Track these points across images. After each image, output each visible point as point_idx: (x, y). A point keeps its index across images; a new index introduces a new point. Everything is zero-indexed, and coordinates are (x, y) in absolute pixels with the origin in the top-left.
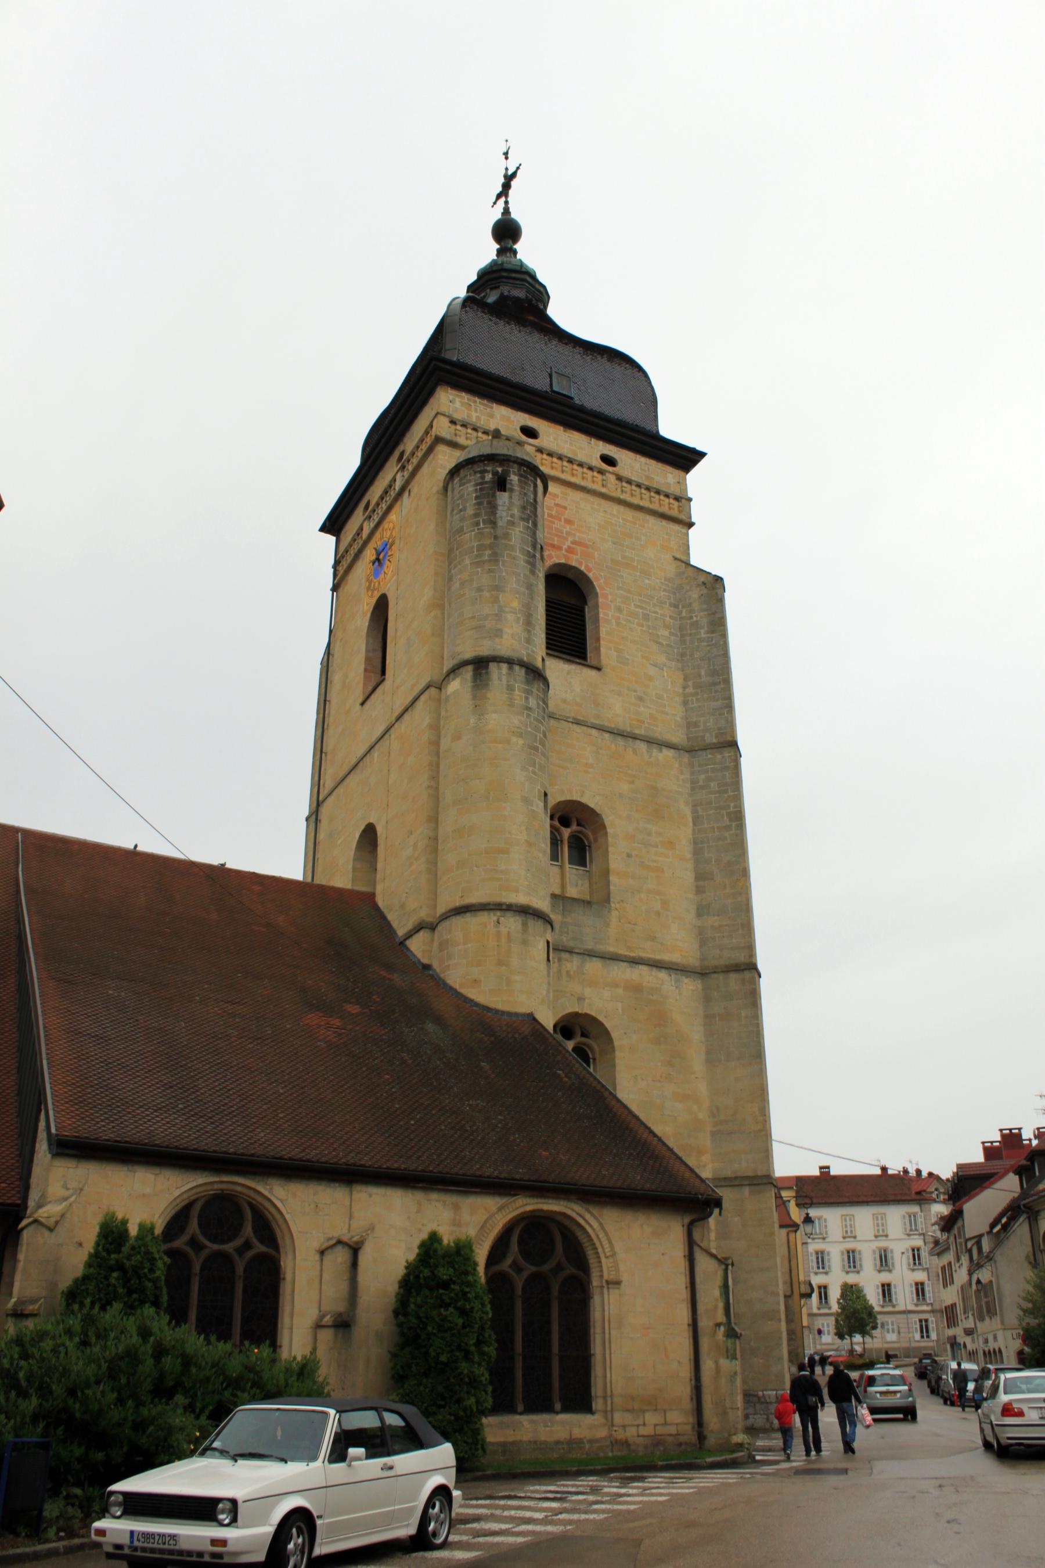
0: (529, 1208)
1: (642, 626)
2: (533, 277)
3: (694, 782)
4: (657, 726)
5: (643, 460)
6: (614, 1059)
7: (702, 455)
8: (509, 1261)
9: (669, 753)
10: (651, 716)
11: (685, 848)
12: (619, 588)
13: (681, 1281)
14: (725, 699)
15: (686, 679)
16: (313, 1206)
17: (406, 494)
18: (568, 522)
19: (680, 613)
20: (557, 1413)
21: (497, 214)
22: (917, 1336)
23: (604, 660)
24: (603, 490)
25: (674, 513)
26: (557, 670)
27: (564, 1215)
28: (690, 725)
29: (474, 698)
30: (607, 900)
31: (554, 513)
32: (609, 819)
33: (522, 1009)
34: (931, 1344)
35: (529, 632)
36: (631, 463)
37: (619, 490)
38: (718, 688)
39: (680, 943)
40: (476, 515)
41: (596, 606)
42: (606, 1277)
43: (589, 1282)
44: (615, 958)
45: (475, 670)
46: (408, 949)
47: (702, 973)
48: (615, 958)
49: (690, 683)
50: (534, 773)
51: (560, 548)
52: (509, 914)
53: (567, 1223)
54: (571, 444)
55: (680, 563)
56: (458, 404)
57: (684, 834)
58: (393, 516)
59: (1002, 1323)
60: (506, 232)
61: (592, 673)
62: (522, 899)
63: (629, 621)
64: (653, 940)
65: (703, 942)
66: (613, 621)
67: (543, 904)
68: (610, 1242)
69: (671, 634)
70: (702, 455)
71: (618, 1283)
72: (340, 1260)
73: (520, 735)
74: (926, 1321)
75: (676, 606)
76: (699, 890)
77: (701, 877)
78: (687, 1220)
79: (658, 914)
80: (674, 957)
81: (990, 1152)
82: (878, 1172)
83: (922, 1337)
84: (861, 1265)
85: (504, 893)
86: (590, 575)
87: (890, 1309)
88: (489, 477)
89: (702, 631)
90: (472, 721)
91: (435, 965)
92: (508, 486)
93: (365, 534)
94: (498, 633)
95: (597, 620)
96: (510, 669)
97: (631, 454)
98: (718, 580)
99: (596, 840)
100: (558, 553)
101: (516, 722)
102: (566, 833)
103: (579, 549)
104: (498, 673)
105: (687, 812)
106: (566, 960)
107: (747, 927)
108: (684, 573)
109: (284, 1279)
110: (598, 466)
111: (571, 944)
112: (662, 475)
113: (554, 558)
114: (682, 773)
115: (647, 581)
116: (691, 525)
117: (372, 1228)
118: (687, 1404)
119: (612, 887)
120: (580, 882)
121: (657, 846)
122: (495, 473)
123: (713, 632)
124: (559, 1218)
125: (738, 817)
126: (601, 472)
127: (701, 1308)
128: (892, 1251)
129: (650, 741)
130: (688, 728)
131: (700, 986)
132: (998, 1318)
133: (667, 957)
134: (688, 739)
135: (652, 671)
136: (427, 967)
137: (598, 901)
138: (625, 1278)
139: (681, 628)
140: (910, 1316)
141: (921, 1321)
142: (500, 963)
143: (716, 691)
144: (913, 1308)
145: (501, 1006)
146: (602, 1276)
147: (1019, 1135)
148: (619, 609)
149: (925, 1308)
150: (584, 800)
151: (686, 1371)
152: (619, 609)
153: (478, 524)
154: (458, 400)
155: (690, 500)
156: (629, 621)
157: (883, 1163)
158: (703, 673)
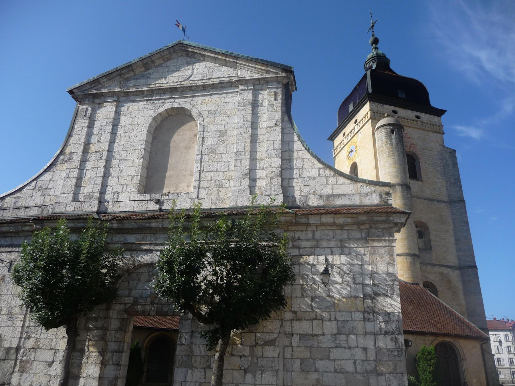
5: (428, 115)
7: (446, 111)
9: (444, 204)
18: (409, 138)
24: (418, 127)
30: (430, 248)
36: (425, 117)
39: (452, 259)
40: (386, 142)
41: (419, 162)
44: (435, 265)
48: (435, 265)
56: (374, 106)
61: (420, 183)
66: (426, 167)
70: (446, 111)
75: (441, 160)
76: (456, 244)
77: (457, 240)
80: (452, 264)
88: (389, 130)
98: (454, 151)
102: (418, 229)
103: (412, 146)
105: (451, 222)
107: (473, 255)
112: (434, 119)
113: (407, 150)
125: (467, 222)
126: (416, 121)
133: (449, 264)
135: (437, 180)
148: (426, 163)
152: (426, 163)
158: (452, 180)
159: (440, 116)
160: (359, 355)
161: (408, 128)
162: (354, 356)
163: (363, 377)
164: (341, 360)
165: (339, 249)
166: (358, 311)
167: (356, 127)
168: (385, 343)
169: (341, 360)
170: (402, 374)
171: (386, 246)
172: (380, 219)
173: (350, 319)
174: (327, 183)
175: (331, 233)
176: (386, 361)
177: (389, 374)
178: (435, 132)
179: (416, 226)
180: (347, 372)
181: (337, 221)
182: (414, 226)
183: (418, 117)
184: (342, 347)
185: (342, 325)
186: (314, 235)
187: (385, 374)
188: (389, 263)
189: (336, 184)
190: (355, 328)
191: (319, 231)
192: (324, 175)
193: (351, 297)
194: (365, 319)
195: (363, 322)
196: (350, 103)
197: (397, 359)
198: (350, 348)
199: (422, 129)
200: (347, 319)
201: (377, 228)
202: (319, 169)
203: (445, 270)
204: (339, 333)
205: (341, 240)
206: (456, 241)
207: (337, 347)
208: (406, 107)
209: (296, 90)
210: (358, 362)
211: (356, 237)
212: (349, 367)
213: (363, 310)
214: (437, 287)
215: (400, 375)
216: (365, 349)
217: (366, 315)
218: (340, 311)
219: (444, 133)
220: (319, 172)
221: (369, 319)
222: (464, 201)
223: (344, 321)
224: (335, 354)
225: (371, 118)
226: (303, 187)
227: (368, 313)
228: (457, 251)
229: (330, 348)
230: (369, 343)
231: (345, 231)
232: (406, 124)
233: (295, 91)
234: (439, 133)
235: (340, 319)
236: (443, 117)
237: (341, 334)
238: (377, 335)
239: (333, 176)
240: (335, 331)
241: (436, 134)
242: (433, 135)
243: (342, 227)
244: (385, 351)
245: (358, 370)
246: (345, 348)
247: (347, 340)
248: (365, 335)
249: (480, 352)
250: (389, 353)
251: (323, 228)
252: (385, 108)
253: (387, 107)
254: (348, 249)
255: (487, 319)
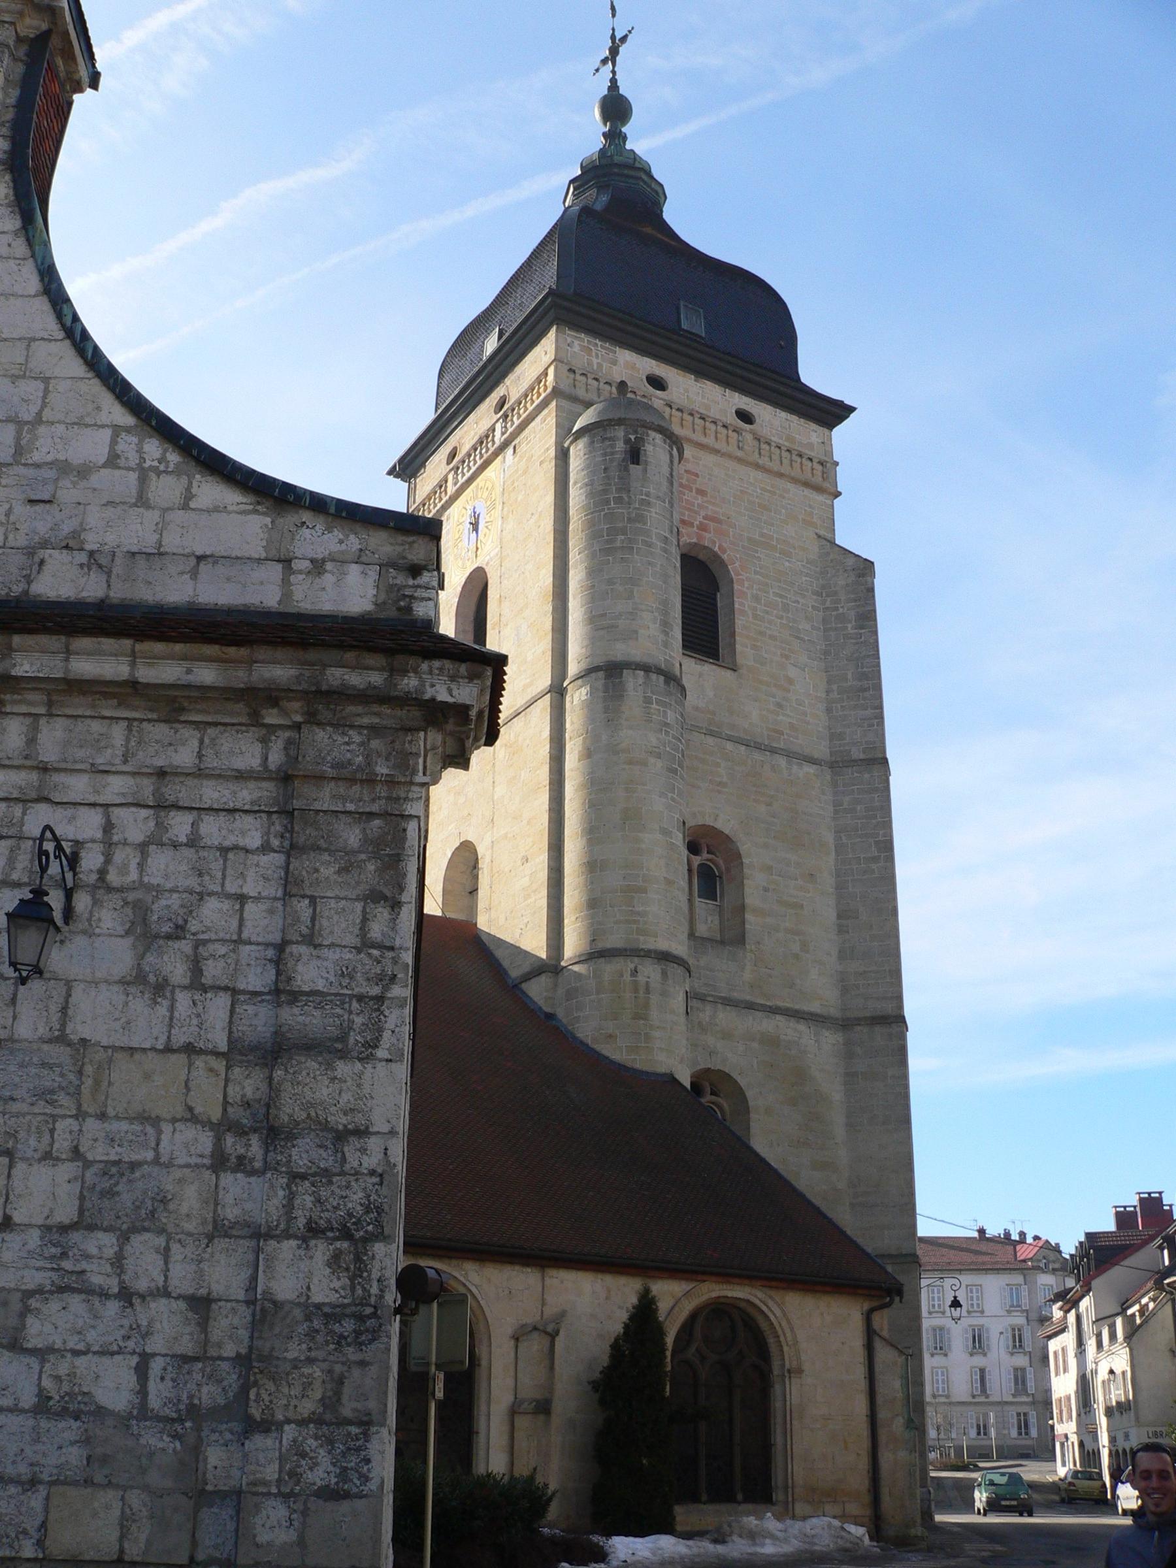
0: (714, 1295)
1: (781, 618)
2: (649, 173)
3: (837, 804)
4: (797, 738)
5: (784, 415)
6: (748, 1121)
7: (852, 409)
8: (693, 1349)
9: (810, 769)
10: (792, 726)
11: (828, 881)
12: (756, 573)
13: (860, 1372)
14: (876, 708)
15: (829, 682)
16: (507, 1292)
17: (510, 451)
18: (701, 492)
19: (824, 602)
20: (739, 1503)
21: (601, 88)
22: (1014, 1433)
23: (740, 660)
24: (739, 454)
25: (818, 479)
26: (698, 675)
27: (748, 1301)
28: (833, 737)
29: (606, 710)
30: (740, 940)
31: (684, 481)
32: (745, 847)
33: (661, 1069)
34: (1029, 1442)
35: (667, 634)
36: (771, 419)
37: (756, 453)
38: (867, 694)
39: (820, 989)
42: (787, 1366)
43: (771, 1371)
44: (750, 1006)
45: (608, 677)
46: (524, 993)
47: (845, 1024)
49: (835, 687)
50: (673, 799)
51: (692, 525)
52: (648, 961)
53: (750, 1310)
54: (703, 397)
55: (825, 542)
56: (576, 348)
57: (828, 862)
58: (490, 472)
59: (1137, 1419)
60: (616, 109)
61: (729, 673)
62: (662, 945)
63: (767, 613)
64: (791, 987)
65: (845, 991)
66: (750, 611)
67: (679, 948)
68: (792, 1329)
69: (813, 628)
70: (852, 409)
71: (800, 1371)
72: (536, 1347)
73: (659, 756)
74: (1025, 1414)
75: (819, 594)
76: (841, 930)
77: (844, 914)
78: (866, 1306)
79: (796, 957)
80: (815, 1007)
81: (1124, 1218)
82: (976, 1235)
83: (1020, 1434)
84: (949, 1345)
85: (642, 938)
86: (725, 557)
87: (982, 1399)
88: (620, 446)
89: (850, 626)
90: (604, 737)
91: (560, 1013)
92: (642, 458)
93: (451, 489)
94: (632, 635)
95: (732, 611)
96: (647, 677)
97: (769, 408)
99: (728, 870)
100: (690, 529)
101: (654, 741)
102: (697, 860)
103: (712, 525)
104: (633, 682)
105: (829, 838)
106: (698, 1009)
108: (828, 554)
109: (479, 1365)
110: (734, 423)
111: (703, 990)
112: (804, 432)
114: (824, 794)
115: (787, 564)
116: (838, 494)
117: (563, 1314)
118: (867, 1499)
119: (747, 926)
120: (710, 919)
121: (796, 879)
122: (627, 441)
123: (862, 627)
124: (742, 1305)
125: (886, 848)
127: (880, 1400)
128: (988, 1330)
129: (790, 755)
130: (831, 740)
131: (841, 1040)
132: (1132, 1413)
134: (831, 754)
136: (550, 1016)
137: (732, 936)
138: (806, 1367)
139: (825, 621)
140: (1006, 1408)
141: (1019, 1414)
142: (637, 1017)
143: (864, 699)
144: (1011, 1399)
145: (638, 1066)
146: (783, 1365)
147: (1160, 1199)
148: (757, 599)
149: (1024, 1399)
150: (719, 825)
151: (864, 1463)
153: (607, 502)
154: (576, 343)
155: (837, 464)
156: (767, 613)
157: (980, 1224)
158: (850, 676)
159: (831, 426)
160: (168, 1326)
161: (701, 454)
162: (146, 1335)
163: (175, 1436)
164: (76, 1353)
165: (144, 813)
166: (191, 1117)
167: (498, 426)
168: (303, 1275)
169: (76, 1353)
170: (360, 1423)
171: (371, 815)
172: (356, 679)
173: (150, 1155)
174: (142, 501)
175: (118, 733)
176: (296, 1364)
177: (302, 1423)
178: (806, 484)
179: (693, 848)
180: (100, 1412)
181: (145, 674)
182: (679, 840)
183: (745, 417)
184: (88, 1291)
185: (106, 1184)
186: (31, 741)
187: (280, 1426)
188: (374, 897)
189: (185, 507)
190: (164, 1201)
191: (60, 723)
192: (133, 460)
193: (168, 1049)
194: (219, 1162)
195: (208, 1175)
196: (488, 332)
197: (351, 1353)
198: (126, 1296)
199: (757, 466)
200: (135, 1157)
201: (341, 725)
202: (117, 430)
203: (789, 1030)
204: (84, 1223)
205: (161, 774)
206: (839, 917)
207: (62, 1290)
208: (701, 371)
209: (94, 85)
210: (156, 1366)
211: (240, 763)
212: (113, 1386)
213: (216, 1115)
214: (749, 1094)
215: (354, 1430)
216: (201, 1305)
217: (229, 1140)
218: (102, 1116)
219: (838, 494)
220: (114, 442)
221: (241, 1158)
222: (880, 763)
223: (117, 1163)
224: (49, 1325)
225: (556, 393)
226: (21, 511)
227: (241, 1132)
228: (842, 955)
229: (28, 1294)
230: (225, 1274)
231: (187, 732)
232: (698, 437)
233: (89, 91)
234: (818, 489)
235: (99, 1152)
236: (837, 431)
237: (91, 1228)
238: (268, 1236)
239: (177, 472)
240: (66, 1213)
241: (808, 492)
242: (796, 493)
243: (172, 704)
244: (298, 1313)
245: (154, 1402)
246: (104, 1295)
247: (118, 1262)
248: (210, 1238)
249: (857, 1343)
250: (316, 1324)
251: (78, 705)
252: (621, 361)
253: (626, 356)
254: (189, 818)
255: (925, 1228)
